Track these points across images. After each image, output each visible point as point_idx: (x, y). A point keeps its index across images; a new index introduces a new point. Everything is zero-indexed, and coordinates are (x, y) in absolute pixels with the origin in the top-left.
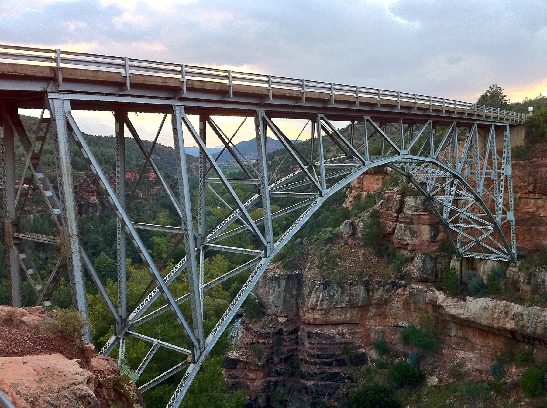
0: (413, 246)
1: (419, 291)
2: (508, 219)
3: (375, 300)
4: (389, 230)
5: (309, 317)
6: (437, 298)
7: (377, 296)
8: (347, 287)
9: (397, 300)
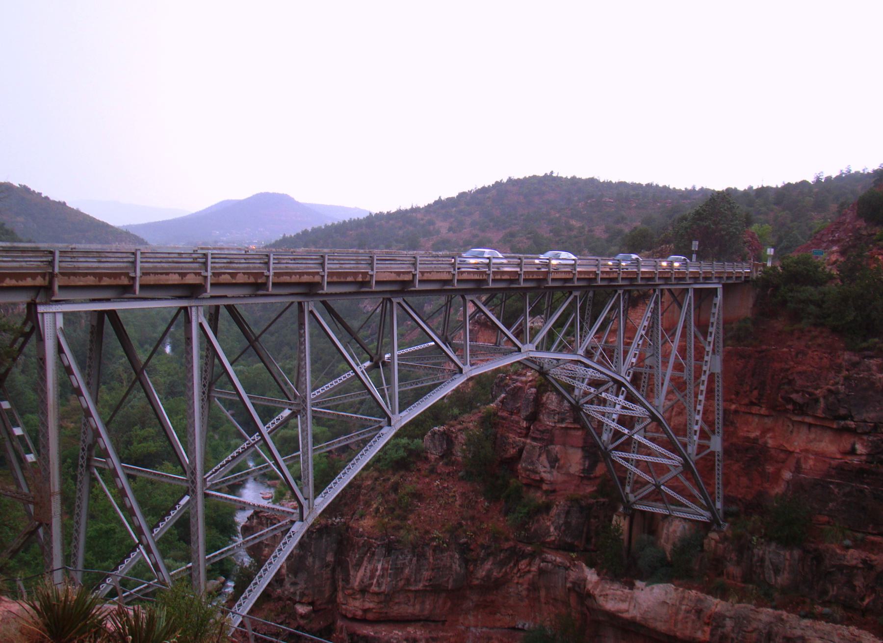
0: (551, 483)
1: (557, 565)
2: (712, 449)
3: (477, 579)
4: (512, 451)
5: (355, 605)
6: (585, 580)
7: (481, 573)
8: (429, 553)
9: (516, 581)
